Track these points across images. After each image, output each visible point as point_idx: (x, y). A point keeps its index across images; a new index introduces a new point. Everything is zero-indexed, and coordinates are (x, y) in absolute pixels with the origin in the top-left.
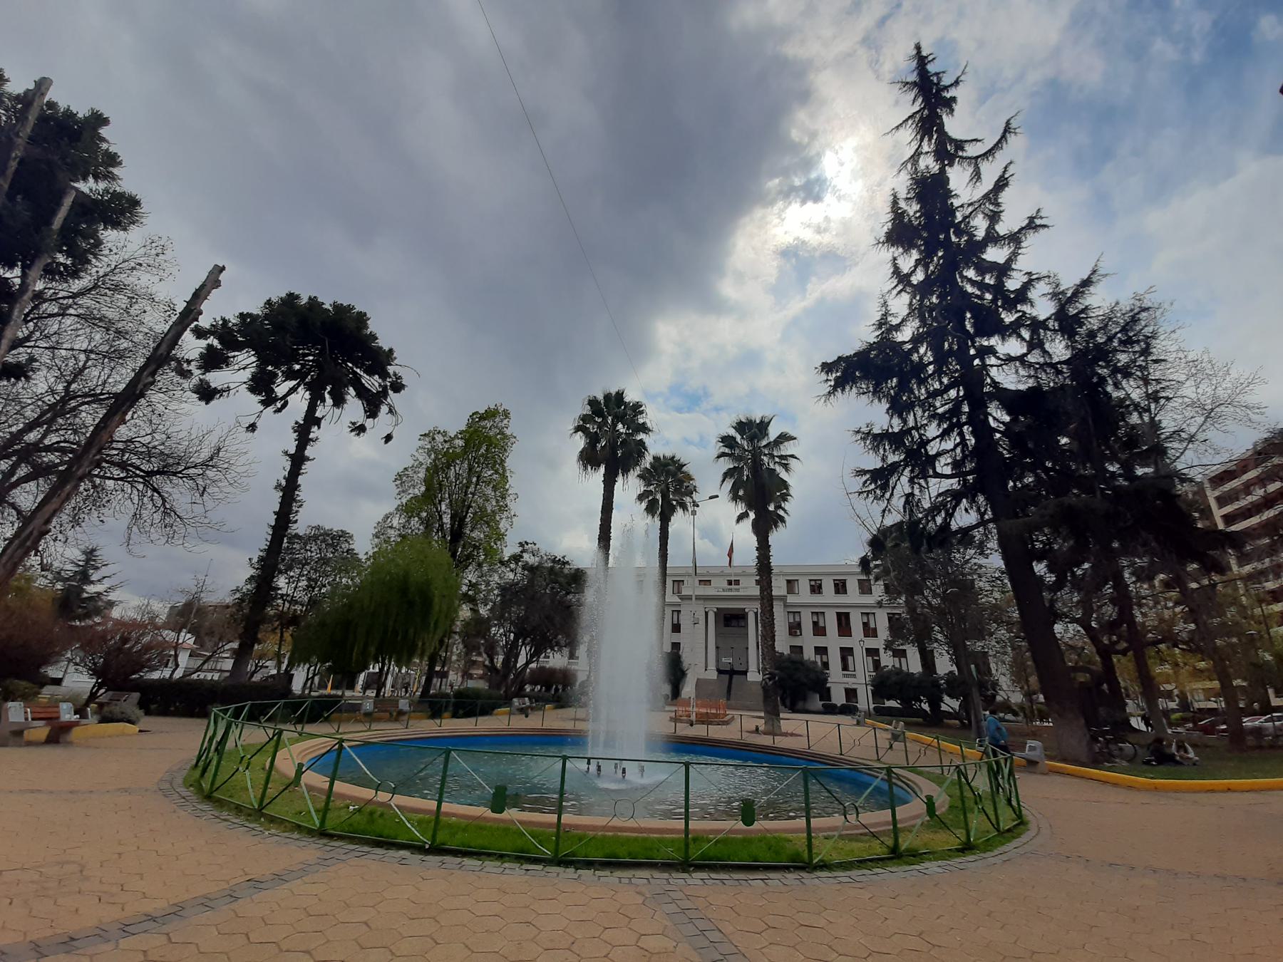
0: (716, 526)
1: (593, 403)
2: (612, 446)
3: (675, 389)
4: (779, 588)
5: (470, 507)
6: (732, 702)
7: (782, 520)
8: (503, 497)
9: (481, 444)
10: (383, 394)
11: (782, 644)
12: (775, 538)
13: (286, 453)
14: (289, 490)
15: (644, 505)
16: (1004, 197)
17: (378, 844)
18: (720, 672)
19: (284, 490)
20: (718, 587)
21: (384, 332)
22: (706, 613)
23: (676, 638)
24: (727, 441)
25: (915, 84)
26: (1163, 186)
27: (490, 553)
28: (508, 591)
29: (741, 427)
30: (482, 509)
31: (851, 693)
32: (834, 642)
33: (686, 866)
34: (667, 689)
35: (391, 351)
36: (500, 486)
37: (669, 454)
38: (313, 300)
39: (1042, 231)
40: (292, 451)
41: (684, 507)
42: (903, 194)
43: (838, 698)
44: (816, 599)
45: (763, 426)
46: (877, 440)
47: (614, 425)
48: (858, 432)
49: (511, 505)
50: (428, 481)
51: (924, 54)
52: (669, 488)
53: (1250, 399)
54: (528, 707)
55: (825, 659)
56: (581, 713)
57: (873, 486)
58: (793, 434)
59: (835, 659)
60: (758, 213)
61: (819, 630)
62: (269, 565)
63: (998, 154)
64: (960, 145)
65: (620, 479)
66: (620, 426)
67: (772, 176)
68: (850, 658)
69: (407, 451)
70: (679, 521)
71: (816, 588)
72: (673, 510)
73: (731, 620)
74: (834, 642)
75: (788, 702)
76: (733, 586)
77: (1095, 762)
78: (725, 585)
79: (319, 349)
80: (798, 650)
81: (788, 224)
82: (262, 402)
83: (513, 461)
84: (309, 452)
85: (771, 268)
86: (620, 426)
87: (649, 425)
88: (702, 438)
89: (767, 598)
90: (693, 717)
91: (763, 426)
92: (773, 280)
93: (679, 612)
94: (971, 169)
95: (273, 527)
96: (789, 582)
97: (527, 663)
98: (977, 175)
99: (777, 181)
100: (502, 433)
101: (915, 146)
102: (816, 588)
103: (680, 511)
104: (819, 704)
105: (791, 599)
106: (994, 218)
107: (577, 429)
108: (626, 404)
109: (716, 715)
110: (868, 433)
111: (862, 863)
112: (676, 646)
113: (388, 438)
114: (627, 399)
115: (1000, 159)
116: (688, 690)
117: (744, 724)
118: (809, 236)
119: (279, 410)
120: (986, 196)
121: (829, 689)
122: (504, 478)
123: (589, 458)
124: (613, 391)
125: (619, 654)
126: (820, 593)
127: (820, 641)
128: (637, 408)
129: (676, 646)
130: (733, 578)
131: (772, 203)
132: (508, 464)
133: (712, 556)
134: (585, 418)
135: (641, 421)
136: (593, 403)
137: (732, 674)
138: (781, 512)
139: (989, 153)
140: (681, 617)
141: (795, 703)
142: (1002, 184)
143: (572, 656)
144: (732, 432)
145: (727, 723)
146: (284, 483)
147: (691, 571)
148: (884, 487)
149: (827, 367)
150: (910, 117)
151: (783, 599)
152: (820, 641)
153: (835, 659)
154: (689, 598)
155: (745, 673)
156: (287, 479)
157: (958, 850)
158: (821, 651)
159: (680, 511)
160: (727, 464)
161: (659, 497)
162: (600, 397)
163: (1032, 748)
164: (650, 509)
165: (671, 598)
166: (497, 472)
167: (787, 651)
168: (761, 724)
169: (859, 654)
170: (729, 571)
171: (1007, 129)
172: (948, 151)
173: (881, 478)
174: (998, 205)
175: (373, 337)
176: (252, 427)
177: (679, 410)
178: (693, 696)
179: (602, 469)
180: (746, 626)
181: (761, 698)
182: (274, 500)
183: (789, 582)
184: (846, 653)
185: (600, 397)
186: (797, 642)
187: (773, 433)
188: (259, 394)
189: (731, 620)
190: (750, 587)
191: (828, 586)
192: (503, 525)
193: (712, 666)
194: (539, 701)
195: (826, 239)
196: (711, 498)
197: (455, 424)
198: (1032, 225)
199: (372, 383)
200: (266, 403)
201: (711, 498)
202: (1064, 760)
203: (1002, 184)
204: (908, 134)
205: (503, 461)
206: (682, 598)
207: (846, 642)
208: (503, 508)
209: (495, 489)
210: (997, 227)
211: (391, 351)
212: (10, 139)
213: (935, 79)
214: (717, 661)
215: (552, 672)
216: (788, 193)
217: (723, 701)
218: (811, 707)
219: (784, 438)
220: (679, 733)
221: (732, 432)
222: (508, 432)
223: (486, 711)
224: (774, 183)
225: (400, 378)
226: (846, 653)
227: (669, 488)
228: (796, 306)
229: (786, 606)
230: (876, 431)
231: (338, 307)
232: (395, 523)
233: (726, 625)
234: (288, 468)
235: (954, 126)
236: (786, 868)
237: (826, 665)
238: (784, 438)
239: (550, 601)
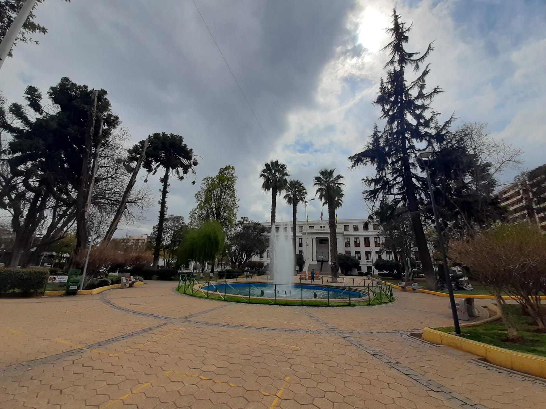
0: (313, 207)
1: (267, 165)
2: (275, 181)
3: (297, 143)
4: (339, 228)
6: (322, 272)
7: (341, 204)
8: (234, 200)
9: (224, 181)
10: (190, 166)
12: (337, 211)
13: (160, 190)
14: (163, 203)
15: (287, 200)
16: (426, 78)
18: (318, 261)
19: (161, 203)
21: (188, 142)
24: (318, 179)
25: (392, 29)
26: (517, 41)
27: (231, 221)
28: (238, 235)
29: (322, 173)
30: (226, 204)
31: (369, 268)
32: (363, 249)
36: (233, 195)
37: (296, 180)
38: (163, 133)
39: (440, 93)
40: (162, 190)
41: (302, 200)
42: (385, 80)
43: (364, 270)
44: (356, 233)
45: (331, 173)
46: (369, 182)
50: (206, 195)
51: (397, 14)
53: (517, 159)
55: (359, 255)
56: (269, 277)
58: (343, 176)
59: (363, 255)
60: (333, 63)
61: (357, 244)
62: (160, 228)
63: (426, 59)
64: (411, 55)
65: (278, 193)
66: (277, 174)
67: (338, 46)
68: (369, 255)
69: (201, 185)
70: (300, 205)
71: (356, 228)
72: (298, 202)
73: (322, 241)
74: (363, 249)
75: (344, 272)
77: (437, 289)
79: (167, 151)
80: (348, 252)
81: (346, 66)
82: (148, 171)
84: (168, 189)
85: (338, 87)
88: (309, 164)
90: (307, 278)
91: (331, 173)
92: (339, 93)
94: (414, 65)
96: (345, 226)
97: (246, 260)
98: (417, 67)
99: (340, 48)
101: (392, 56)
103: (301, 202)
105: (346, 233)
106: (422, 87)
107: (261, 176)
108: (279, 165)
113: (194, 183)
114: (279, 163)
115: (427, 60)
116: (305, 268)
118: (357, 73)
119: (154, 174)
120: (419, 79)
123: (266, 186)
124: (274, 161)
125: (281, 254)
126: (358, 230)
127: (357, 249)
128: (283, 166)
129: (301, 252)
130: (322, 225)
131: (339, 58)
132: (235, 187)
133: (314, 218)
134: (264, 171)
135: (285, 172)
136: (267, 165)
137: (322, 262)
139: (422, 58)
141: (347, 271)
142: (425, 73)
143: (261, 257)
144: (319, 175)
145: (319, 279)
146: (161, 201)
147: (306, 223)
148: (374, 197)
149: (351, 158)
150: (390, 44)
151: (342, 233)
152: (357, 249)
153: (363, 255)
154: (305, 234)
155: (328, 261)
158: (358, 252)
159: (301, 202)
160: (317, 187)
161: (292, 196)
162: (270, 163)
163: (414, 285)
164: (289, 201)
167: (344, 253)
168: (330, 280)
169: (373, 254)
171: (429, 48)
172: (404, 58)
174: (424, 81)
176: (146, 181)
177: (300, 152)
179: (271, 189)
182: (158, 208)
183: (345, 226)
184: (368, 253)
185: (270, 163)
186: (348, 249)
189: (322, 241)
191: (351, 228)
192: (235, 210)
193: (315, 259)
195: (363, 73)
197: (215, 173)
198: (436, 91)
199: (185, 161)
200: (150, 171)
202: (425, 289)
203: (425, 73)
204: (390, 50)
205: (233, 187)
207: (368, 249)
208: (235, 204)
209: (231, 197)
210: (423, 91)
211: (191, 150)
212: (91, 114)
213: (401, 26)
214: (317, 257)
216: (345, 53)
218: (353, 273)
219: (339, 177)
221: (319, 175)
222: (234, 175)
224: (339, 49)
227: (296, 193)
228: (350, 103)
230: (370, 179)
232: (196, 212)
233: (320, 243)
235: (407, 47)
237: (360, 258)
238: (339, 177)
239: (255, 238)
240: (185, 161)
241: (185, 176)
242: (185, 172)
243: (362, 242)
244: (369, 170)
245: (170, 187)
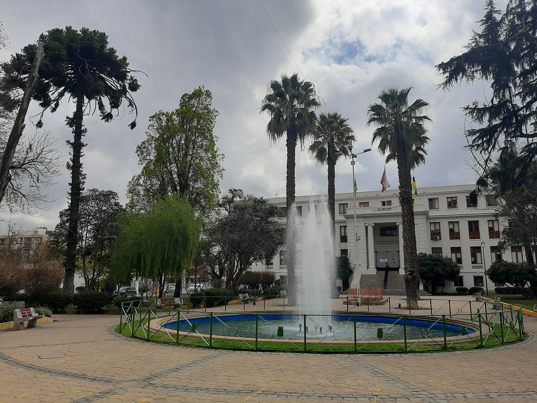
0: (368, 166)
1: (275, 86)
4: (420, 205)
5: (190, 165)
6: (388, 290)
7: (422, 158)
8: (214, 157)
9: (192, 119)
10: (123, 91)
11: (424, 246)
13: (68, 142)
14: (76, 167)
17: (235, 349)
18: (378, 269)
20: (375, 207)
21: (119, 45)
22: (366, 228)
23: (344, 246)
24: (376, 109)
27: (209, 198)
29: (385, 97)
31: (478, 280)
32: (466, 243)
33: (356, 352)
34: (339, 283)
35: (125, 59)
36: (210, 147)
37: (332, 113)
38: (69, 29)
40: (73, 141)
43: (469, 283)
44: (453, 212)
45: (403, 96)
46: (477, 112)
47: (292, 102)
48: (467, 108)
49: (220, 163)
52: (333, 139)
54: (248, 300)
55: (459, 256)
57: (480, 142)
61: (454, 235)
62: (73, 216)
65: (298, 142)
66: (296, 103)
68: (478, 255)
69: (145, 131)
70: (343, 164)
73: (385, 231)
74: (466, 243)
75: (430, 288)
76: (386, 207)
78: (380, 205)
80: (437, 250)
82: (41, 105)
83: (220, 130)
84: (83, 140)
86: (296, 103)
87: (317, 101)
89: (409, 215)
90: (359, 301)
91: (403, 96)
93: (345, 227)
95: (71, 194)
96: (430, 200)
100: (206, 108)
102: (452, 204)
104: (453, 288)
105: (432, 213)
108: (299, 85)
109: (374, 299)
110: (475, 109)
111: (429, 351)
112: (344, 252)
113: (133, 125)
116: (355, 283)
117: (395, 303)
119: (54, 110)
121: (461, 278)
122: (212, 143)
123: (275, 129)
127: (455, 243)
129: (344, 252)
130: (386, 200)
133: (370, 186)
134: (269, 98)
135: (311, 98)
136: (275, 86)
137: (386, 270)
138: (421, 152)
140: (348, 231)
144: (379, 102)
145: (382, 304)
148: (489, 142)
152: (455, 243)
154: (352, 217)
155: (397, 269)
156: (73, 161)
157: (475, 348)
158: (456, 250)
161: (326, 146)
162: (280, 81)
164: (320, 157)
165: (339, 217)
166: (206, 138)
167: (429, 252)
168: (404, 304)
170: (384, 194)
173: (486, 137)
175: (112, 51)
178: (358, 287)
179: (285, 136)
180: (397, 235)
181: (404, 286)
183: (430, 200)
184: (475, 251)
185: (280, 81)
186: (437, 245)
187: (411, 101)
188: (40, 100)
189: (385, 231)
190: (397, 207)
192: (217, 177)
193: (372, 265)
194: (255, 295)
196: (365, 151)
197: (172, 105)
199: (112, 83)
201: (365, 151)
205: (210, 131)
206: (348, 217)
207: (476, 243)
208: (215, 165)
209: (206, 151)
211: (125, 59)
214: (376, 262)
215: (257, 275)
217: (379, 290)
219: (419, 104)
220: (350, 310)
221: (379, 102)
222: (211, 108)
223: (223, 303)
225: (136, 80)
226: (475, 251)
227: (333, 139)
229: (428, 218)
230: (480, 106)
231: (85, 31)
234: (72, 153)
236: (396, 353)
237: (459, 261)
238: (419, 104)
240: (112, 83)
241: (114, 112)
242: (115, 104)
243: (464, 229)
244: (480, 89)
245: (87, 134)
